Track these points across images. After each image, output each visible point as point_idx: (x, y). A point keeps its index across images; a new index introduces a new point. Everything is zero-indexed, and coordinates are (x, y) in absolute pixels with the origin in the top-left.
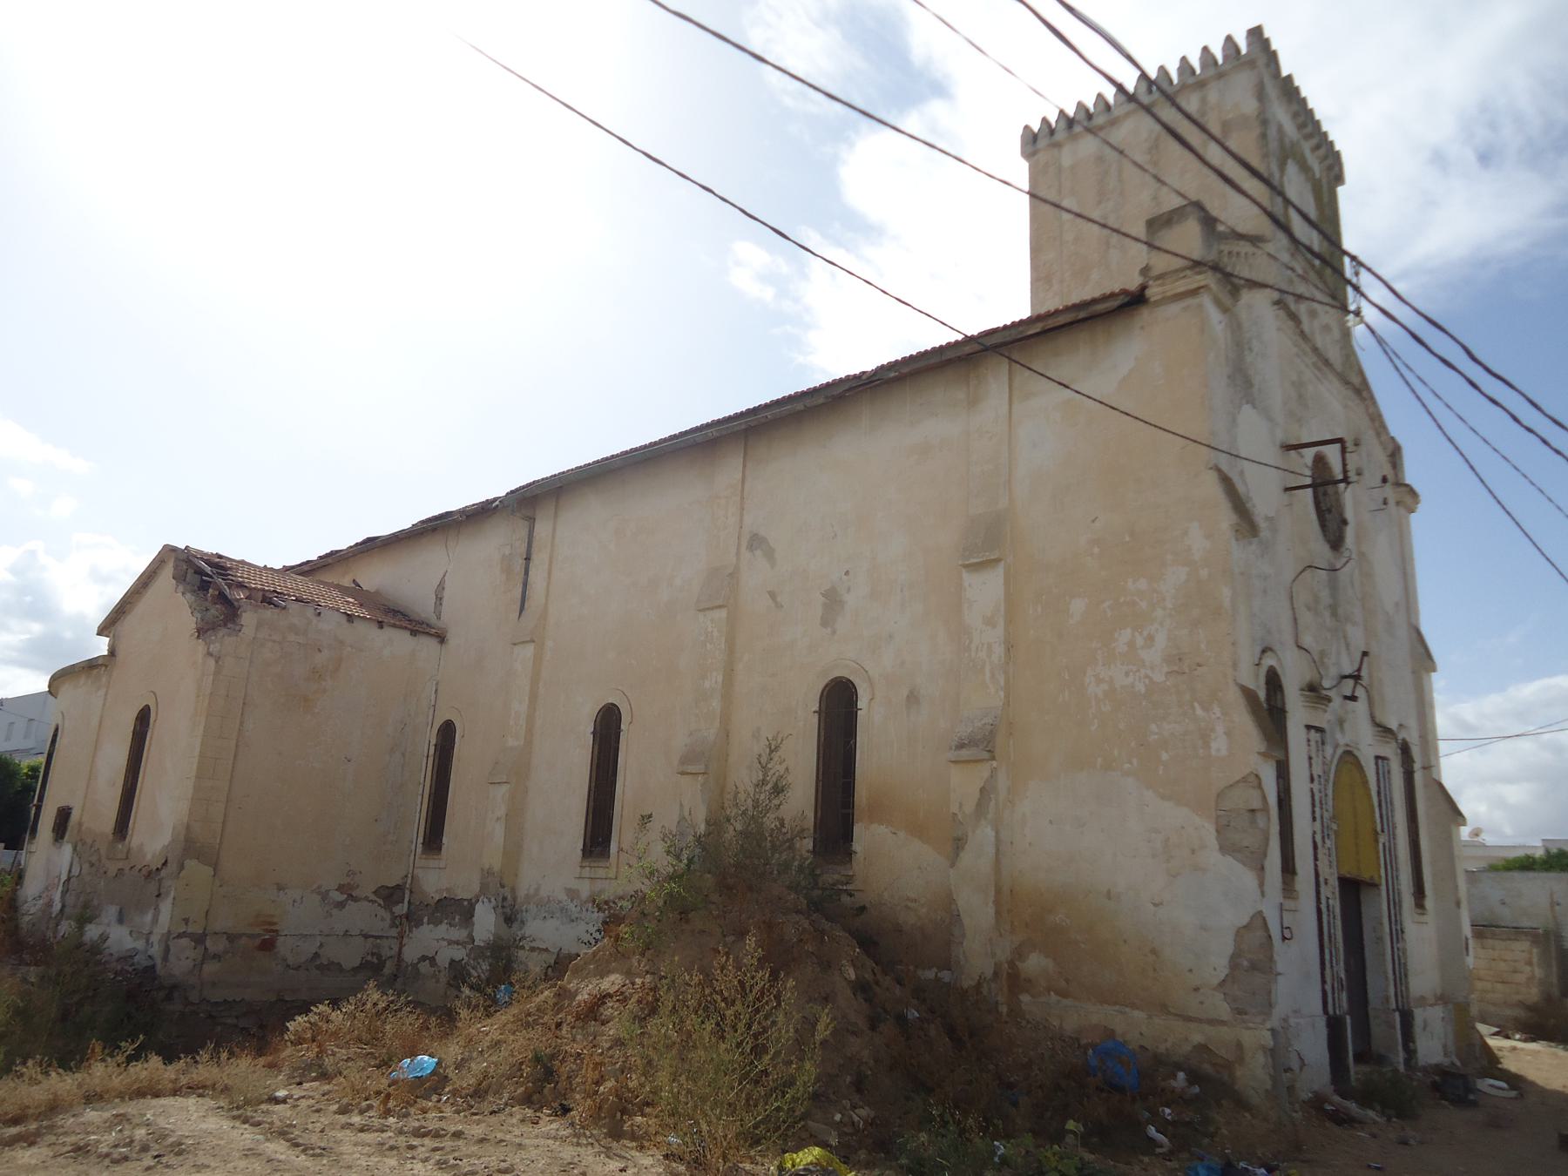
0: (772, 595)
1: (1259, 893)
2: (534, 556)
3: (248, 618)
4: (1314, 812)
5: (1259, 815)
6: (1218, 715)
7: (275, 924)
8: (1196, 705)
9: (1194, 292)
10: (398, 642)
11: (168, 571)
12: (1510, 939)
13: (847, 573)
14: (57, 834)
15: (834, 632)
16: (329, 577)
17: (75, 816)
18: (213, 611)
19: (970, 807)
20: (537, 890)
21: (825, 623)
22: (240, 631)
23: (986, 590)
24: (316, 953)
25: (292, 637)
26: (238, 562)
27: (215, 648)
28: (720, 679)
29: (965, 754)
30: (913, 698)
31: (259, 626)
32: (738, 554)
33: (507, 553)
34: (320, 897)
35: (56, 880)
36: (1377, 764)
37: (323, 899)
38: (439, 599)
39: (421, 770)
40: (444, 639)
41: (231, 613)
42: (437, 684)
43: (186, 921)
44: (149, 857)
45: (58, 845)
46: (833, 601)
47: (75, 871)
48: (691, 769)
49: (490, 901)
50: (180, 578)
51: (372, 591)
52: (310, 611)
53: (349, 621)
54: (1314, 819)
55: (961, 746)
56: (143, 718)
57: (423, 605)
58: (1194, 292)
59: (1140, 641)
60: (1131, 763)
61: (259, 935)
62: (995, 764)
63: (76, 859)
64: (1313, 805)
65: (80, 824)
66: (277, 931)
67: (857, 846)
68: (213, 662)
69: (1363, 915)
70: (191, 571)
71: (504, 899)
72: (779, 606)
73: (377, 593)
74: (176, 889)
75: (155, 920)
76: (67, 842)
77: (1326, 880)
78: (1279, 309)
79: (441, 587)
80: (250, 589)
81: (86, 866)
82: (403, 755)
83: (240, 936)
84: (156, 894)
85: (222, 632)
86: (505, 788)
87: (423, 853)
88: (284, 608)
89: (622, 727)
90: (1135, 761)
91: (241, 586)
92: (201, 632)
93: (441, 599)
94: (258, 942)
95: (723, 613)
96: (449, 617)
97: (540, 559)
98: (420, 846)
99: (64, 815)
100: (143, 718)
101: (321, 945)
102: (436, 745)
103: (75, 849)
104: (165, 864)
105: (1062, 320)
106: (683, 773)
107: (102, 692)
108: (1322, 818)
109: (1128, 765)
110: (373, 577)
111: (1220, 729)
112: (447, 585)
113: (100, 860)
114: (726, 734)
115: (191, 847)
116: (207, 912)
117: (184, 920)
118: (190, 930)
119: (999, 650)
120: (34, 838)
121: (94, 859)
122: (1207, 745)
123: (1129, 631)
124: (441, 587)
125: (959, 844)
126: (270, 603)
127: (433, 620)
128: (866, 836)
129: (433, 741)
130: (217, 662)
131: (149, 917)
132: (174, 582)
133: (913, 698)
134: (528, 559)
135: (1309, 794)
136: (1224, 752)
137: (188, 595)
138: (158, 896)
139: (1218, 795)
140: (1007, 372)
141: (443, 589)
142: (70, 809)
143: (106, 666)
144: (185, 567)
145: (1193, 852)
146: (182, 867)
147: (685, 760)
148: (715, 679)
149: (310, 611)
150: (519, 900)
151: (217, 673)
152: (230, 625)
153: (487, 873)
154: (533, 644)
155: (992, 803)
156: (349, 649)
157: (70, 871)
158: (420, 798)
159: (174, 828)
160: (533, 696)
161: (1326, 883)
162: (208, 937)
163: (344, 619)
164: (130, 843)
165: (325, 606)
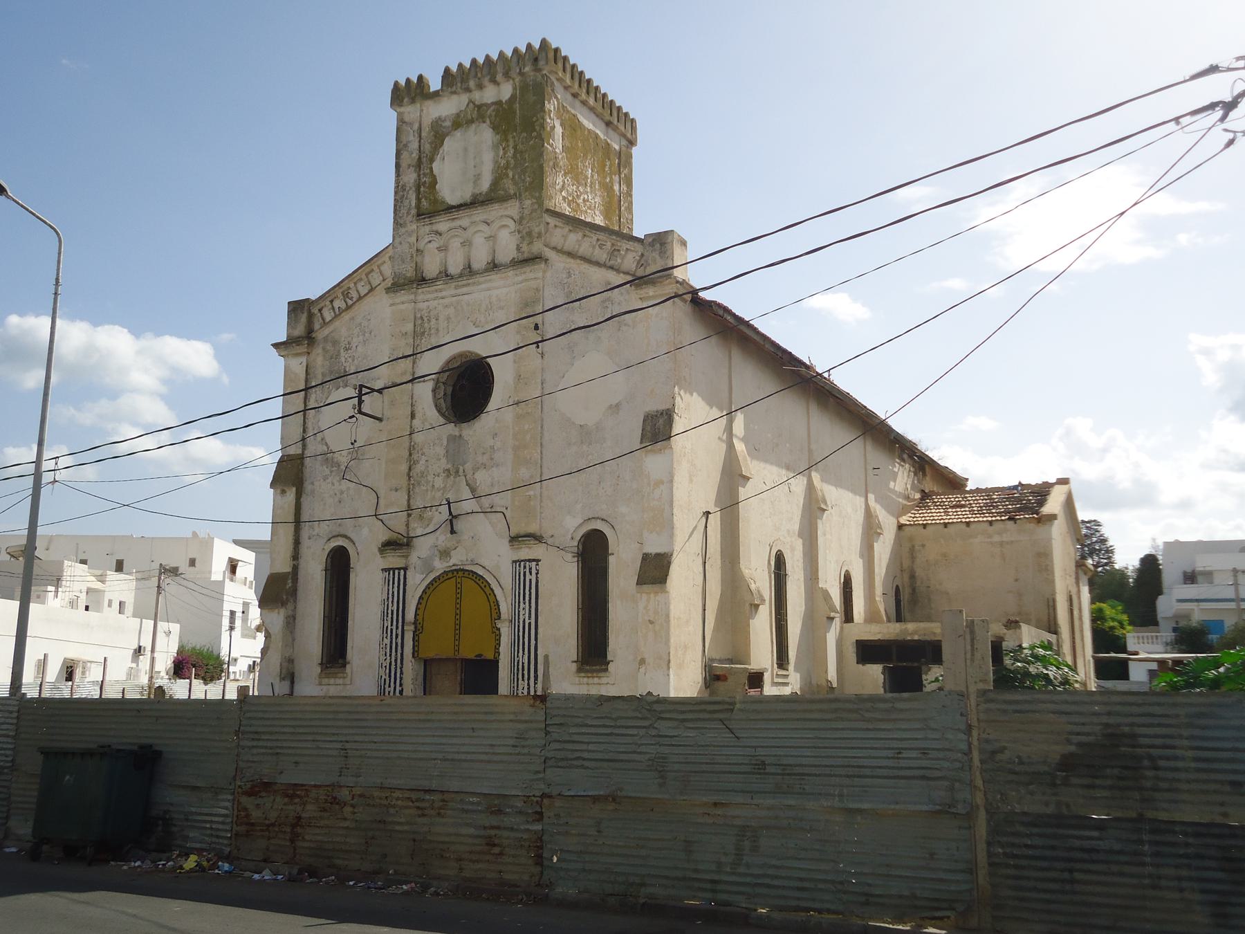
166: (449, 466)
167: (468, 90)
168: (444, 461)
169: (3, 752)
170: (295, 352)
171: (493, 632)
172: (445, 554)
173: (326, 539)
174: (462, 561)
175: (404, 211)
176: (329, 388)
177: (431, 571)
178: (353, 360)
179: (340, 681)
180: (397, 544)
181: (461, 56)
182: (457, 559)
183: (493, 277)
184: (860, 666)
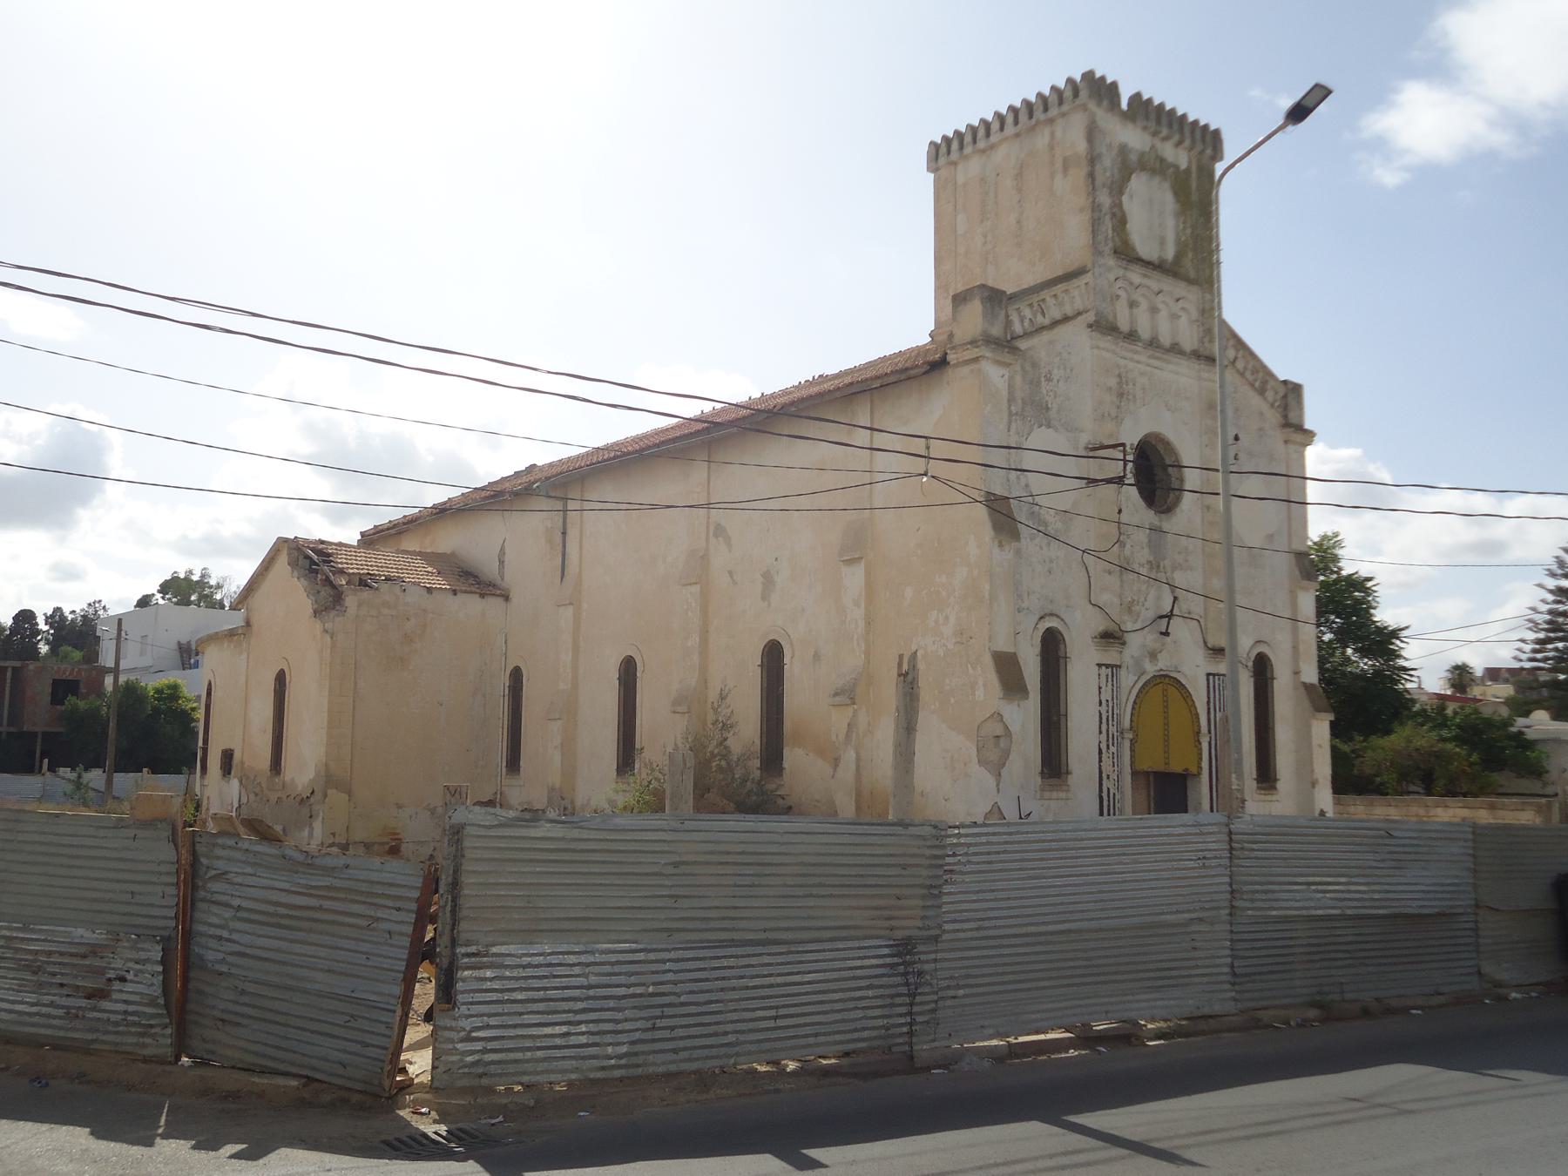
0: (730, 573)
1: (996, 791)
2: (569, 531)
3: (350, 601)
4: (1100, 728)
5: (1002, 739)
6: (980, 672)
7: (398, 834)
8: (969, 666)
9: (976, 360)
10: (470, 606)
11: (283, 560)
12: (1517, 810)
13: (776, 559)
14: (224, 771)
15: (769, 605)
16: (412, 544)
17: (237, 756)
18: (323, 593)
19: (842, 737)
20: (589, 800)
21: (765, 597)
22: (345, 611)
23: (854, 579)
24: (431, 855)
25: (386, 611)
26: (336, 544)
27: (328, 626)
28: (698, 639)
29: (838, 699)
30: (817, 657)
31: (359, 605)
32: (707, 539)
33: (549, 526)
34: (429, 813)
35: (230, 808)
36: (1208, 680)
37: (433, 813)
38: (502, 562)
39: (499, 707)
40: (508, 597)
41: (337, 598)
42: (506, 636)
43: (334, 834)
44: (300, 788)
45: (226, 779)
46: (768, 580)
47: (244, 800)
48: (679, 709)
49: (555, 811)
50: (293, 564)
51: (449, 552)
52: (397, 589)
53: (428, 593)
54: (1100, 732)
55: (836, 694)
56: (281, 679)
57: (490, 569)
58: (976, 360)
59: (941, 621)
60: (935, 705)
61: (388, 843)
62: (855, 706)
63: (243, 791)
64: (1101, 722)
65: (242, 763)
66: (400, 839)
67: (786, 764)
68: (329, 639)
69: (1189, 799)
70: (301, 557)
71: (565, 809)
72: (735, 583)
73: (453, 554)
74: (323, 812)
75: (311, 835)
76: (235, 777)
77: (1108, 775)
78: (1092, 331)
79: (502, 551)
80: (349, 574)
81: (252, 797)
82: (484, 696)
83: (374, 844)
84: (309, 815)
85: (333, 613)
86: (560, 722)
87: (507, 774)
88: (377, 589)
89: (638, 675)
90: (937, 704)
91: (342, 572)
92: (316, 613)
93: (503, 562)
94: (387, 847)
95: (696, 589)
96: (511, 579)
97: (572, 533)
98: (504, 769)
99: (228, 756)
100: (281, 679)
101: (435, 849)
102: (509, 687)
103: (241, 782)
104: (313, 792)
105: (892, 379)
106: (674, 712)
107: (244, 656)
108: (1108, 731)
109: (933, 707)
110: (448, 540)
111: (980, 683)
112: (507, 551)
113: (262, 791)
114: (704, 681)
115: (330, 780)
116: (348, 827)
117: (332, 834)
118: (337, 842)
119: (862, 624)
120: (206, 773)
121: (257, 790)
122: (973, 694)
123: (936, 612)
124: (502, 551)
125: (836, 762)
126: (366, 585)
127: (498, 581)
128: (793, 757)
129: (507, 684)
130: (332, 638)
131: (306, 833)
132: (289, 568)
133: (817, 657)
134: (564, 533)
135: (1098, 714)
136: (982, 698)
137: (302, 579)
138: (311, 817)
139: (978, 727)
140: (869, 410)
141: (504, 553)
142: (233, 751)
143: (244, 634)
144: (296, 554)
145: (965, 764)
146: (325, 796)
147: (676, 702)
148: (694, 640)
149: (397, 589)
150: (577, 808)
151: (333, 647)
152: (338, 608)
153: (552, 789)
154: (572, 606)
155: (854, 735)
156: (431, 615)
157: (240, 801)
158: (501, 730)
159: (316, 766)
160: (576, 649)
161: (1108, 778)
162: (351, 846)
163: (424, 592)
164: (284, 777)
165: (409, 582)
166: (1151, 558)
167: (1155, 134)
168: (1146, 550)
169: (2, 991)
170: (999, 358)
171: (1196, 746)
172: (1153, 656)
173: (1037, 617)
174: (1167, 667)
175: (1101, 237)
176: (1030, 421)
177: (1142, 674)
178: (1055, 397)
179: (1063, 795)
180: (1111, 637)
181: (1158, 94)
182: (1163, 663)
183: (1182, 362)
184: (1279, 785)
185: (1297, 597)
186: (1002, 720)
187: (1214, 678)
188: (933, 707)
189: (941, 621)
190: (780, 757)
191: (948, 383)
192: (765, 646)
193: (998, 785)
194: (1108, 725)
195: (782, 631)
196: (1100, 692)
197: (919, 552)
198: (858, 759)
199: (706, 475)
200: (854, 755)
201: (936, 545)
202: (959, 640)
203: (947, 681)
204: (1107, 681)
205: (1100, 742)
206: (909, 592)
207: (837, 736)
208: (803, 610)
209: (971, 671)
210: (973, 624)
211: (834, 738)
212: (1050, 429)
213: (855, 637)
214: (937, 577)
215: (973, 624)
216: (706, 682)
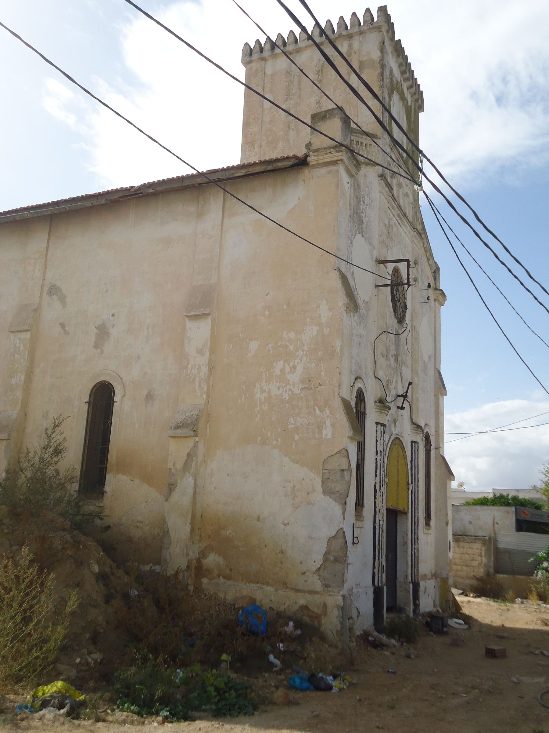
0: (63, 326)
4: (376, 472)
6: (328, 414)
8: (316, 408)
15: (102, 352)
19: (179, 466)
21: (97, 346)
28: (23, 378)
29: (179, 432)
30: (150, 397)
36: (412, 446)
54: (376, 476)
55: (177, 427)
58: (335, 163)
59: (288, 369)
60: (277, 441)
64: (376, 468)
72: (66, 333)
90: (279, 440)
105: (257, 169)
108: (380, 475)
109: (275, 442)
111: (328, 423)
122: (320, 432)
123: (282, 362)
133: (150, 397)
135: (375, 461)
136: (329, 436)
148: (20, 378)
155: (194, 463)
161: (380, 512)
185: (439, 399)
186: (348, 456)
187: (415, 444)
188: (275, 442)
189: (288, 369)
190: (102, 481)
191: (304, 180)
192: (94, 387)
193: (344, 513)
194: (381, 469)
195: (115, 374)
196: (377, 445)
197: (267, 313)
198: (195, 485)
199: (45, 245)
200: (193, 481)
201: (285, 307)
202: (307, 386)
203: (292, 420)
204: (381, 437)
205: (376, 483)
206: (254, 346)
207: (174, 464)
208: (138, 357)
209: (318, 412)
210: (323, 373)
211: (170, 465)
212: (363, 238)
213: (197, 380)
214: (285, 333)
215: (323, 373)
216: (26, 415)
